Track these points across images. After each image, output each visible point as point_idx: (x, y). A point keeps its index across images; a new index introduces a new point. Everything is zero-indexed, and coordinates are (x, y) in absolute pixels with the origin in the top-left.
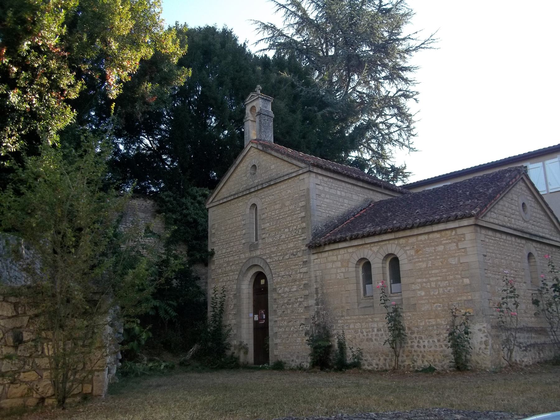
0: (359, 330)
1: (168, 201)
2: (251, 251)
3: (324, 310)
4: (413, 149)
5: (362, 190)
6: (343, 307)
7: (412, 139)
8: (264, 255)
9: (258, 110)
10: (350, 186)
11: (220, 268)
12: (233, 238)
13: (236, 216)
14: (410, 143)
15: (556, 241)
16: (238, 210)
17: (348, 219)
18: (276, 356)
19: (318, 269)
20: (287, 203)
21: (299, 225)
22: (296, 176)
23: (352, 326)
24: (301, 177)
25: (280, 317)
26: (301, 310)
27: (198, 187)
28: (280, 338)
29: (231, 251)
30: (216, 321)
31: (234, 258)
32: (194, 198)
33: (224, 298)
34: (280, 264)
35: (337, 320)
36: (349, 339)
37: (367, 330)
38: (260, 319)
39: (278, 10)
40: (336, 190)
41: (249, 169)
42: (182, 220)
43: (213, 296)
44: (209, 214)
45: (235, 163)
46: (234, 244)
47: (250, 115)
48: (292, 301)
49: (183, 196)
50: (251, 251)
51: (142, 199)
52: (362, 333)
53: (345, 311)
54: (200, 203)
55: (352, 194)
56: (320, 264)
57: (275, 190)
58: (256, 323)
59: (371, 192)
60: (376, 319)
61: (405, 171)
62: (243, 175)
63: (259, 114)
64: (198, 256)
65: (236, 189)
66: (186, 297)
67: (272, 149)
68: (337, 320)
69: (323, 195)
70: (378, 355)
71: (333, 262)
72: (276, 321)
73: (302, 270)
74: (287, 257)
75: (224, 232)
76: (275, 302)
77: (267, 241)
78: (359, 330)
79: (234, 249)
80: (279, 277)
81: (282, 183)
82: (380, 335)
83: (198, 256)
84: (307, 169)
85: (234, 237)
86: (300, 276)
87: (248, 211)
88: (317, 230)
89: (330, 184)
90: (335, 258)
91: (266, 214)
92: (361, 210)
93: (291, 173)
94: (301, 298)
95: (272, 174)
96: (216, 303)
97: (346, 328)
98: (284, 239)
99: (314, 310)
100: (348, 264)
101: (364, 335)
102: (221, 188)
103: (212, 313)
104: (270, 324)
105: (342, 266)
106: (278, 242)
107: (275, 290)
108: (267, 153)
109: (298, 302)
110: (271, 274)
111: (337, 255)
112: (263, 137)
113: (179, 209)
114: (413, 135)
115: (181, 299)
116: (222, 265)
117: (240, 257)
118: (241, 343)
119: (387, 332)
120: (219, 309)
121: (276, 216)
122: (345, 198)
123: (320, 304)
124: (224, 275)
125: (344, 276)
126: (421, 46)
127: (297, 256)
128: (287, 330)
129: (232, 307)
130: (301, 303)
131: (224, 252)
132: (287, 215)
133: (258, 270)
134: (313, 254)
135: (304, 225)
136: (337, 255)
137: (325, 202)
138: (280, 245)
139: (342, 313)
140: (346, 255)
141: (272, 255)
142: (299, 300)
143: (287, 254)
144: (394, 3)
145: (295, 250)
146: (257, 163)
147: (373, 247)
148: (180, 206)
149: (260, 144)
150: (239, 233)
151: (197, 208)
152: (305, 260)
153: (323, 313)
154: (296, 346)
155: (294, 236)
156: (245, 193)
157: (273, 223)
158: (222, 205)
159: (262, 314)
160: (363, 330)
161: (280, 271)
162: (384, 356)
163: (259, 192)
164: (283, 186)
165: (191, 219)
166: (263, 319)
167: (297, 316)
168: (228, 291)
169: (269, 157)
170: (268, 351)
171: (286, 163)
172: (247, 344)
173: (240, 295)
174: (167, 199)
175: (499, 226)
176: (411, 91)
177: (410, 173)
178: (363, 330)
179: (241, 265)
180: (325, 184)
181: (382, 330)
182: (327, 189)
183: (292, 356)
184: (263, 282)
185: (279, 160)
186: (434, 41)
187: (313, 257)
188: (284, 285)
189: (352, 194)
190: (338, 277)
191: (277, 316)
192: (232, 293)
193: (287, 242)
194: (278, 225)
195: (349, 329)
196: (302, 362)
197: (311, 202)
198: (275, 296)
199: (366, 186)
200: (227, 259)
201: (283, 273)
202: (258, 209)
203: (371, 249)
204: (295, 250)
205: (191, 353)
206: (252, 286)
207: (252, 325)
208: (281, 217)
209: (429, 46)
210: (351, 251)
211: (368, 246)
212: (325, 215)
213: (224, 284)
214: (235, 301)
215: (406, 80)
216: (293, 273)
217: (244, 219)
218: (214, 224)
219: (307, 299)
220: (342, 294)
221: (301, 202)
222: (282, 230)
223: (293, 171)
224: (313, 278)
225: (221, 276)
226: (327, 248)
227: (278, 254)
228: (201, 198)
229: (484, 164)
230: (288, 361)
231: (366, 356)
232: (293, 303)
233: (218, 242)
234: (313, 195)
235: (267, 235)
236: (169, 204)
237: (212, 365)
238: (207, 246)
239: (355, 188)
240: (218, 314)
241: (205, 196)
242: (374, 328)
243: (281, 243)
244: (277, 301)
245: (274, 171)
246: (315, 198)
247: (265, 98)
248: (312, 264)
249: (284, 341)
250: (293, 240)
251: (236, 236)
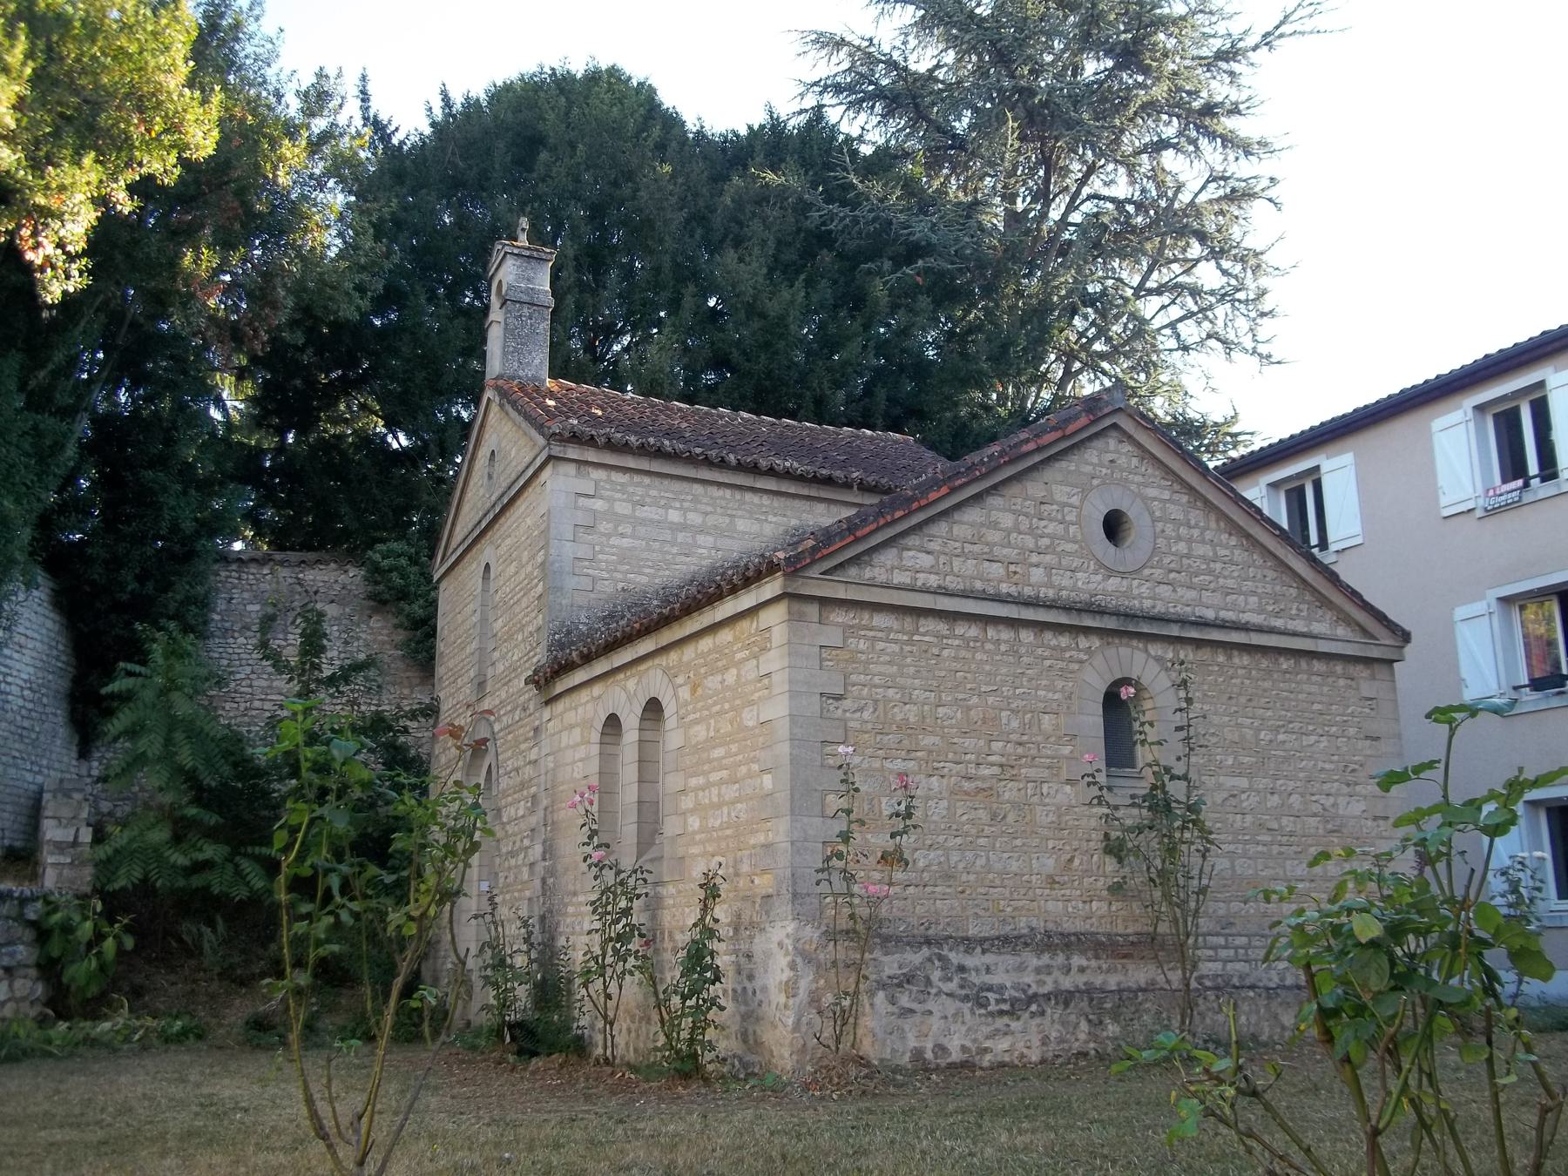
5: (778, 503)
7: (1266, 327)
15: (1295, 634)
51: (333, 565)
55: (730, 516)
57: (509, 523)
61: (1234, 430)
89: (640, 491)
122: (702, 530)
126: (1281, 30)
137: (613, 546)
175: (927, 596)
177: (1252, 434)
182: (623, 508)
189: (730, 516)
199: (792, 488)
209: (1308, 25)
212: (607, 588)
215: (1228, 140)
236: (394, 575)
239: (749, 496)
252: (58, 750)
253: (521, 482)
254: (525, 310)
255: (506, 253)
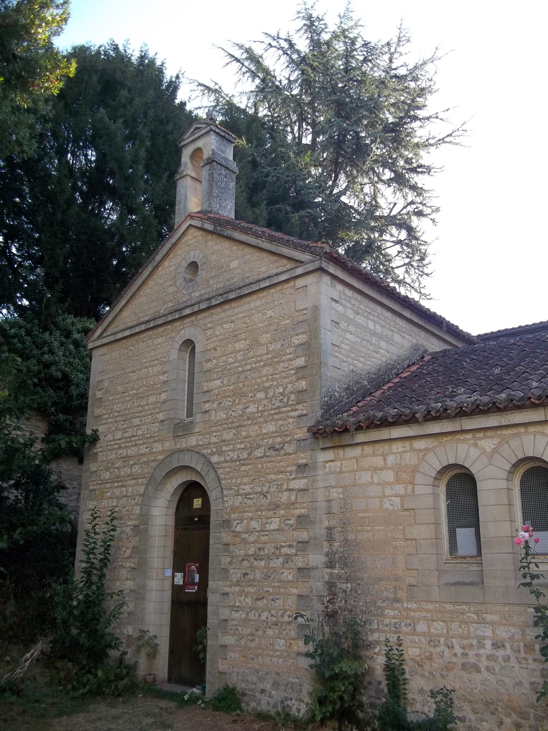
0: (442, 640)
1: (15, 336)
2: (176, 437)
3: (347, 580)
4: (425, 295)
5: (409, 327)
6: (397, 579)
7: (424, 281)
8: (206, 446)
9: (206, 154)
10: (389, 315)
11: (107, 469)
12: (140, 409)
13: (148, 364)
14: (421, 286)
16: (153, 353)
17: (389, 382)
18: (222, 673)
19: (334, 484)
20: (265, 338)
21: (290, 386)
22: (286, 281)
23: (421, 627)
24: (300, 282)
25: (236, 586)
26: (288, 575)
27: (75, 316)
28: (234, 634)
29: (133, 436)
30: (92, 584)
31: (138, 450)
32: (68, 334)
33: (112, 533)
34: (243, 468)
35: (383, 609)
36: (413, 660)
37: (465, 642)
38: (188, 582)
39: (227, 64)
40: (366, 317)
41: (182, 270)
42: (39, 373)
43: (89, 527)
44: (93, 364)
45: (154, 259)
46: (141, 421)
47: (190, 165)
48: (266, 551)
49: (45, 329)
50: (176, 437)
52: (451, 647)
53: (405, 589)
54: (77, 344)
55: (392, 331)
56: (341, 472)
57: (237, 311)
58: (176, 590)
59: (423, 334)
60: (489, 617)
62: (169, 283)
63: (210, 161)
64: (63, 443)
65: (151, 312)
66: (29, 528)
67: (235, 228)
68: (381, 607)
69: (343, 325)
70: (497, 710)
71: (376, 469)
72: (226, 594)
73: (292, 485)
74: (258, 453)
75: (122, 397)
76: (227, 550)
77: (213, 416)
78: (442, 640)
79: (140, 432)
80: (236, 495)
81: (254, 297)
82: (500, 659)
83: (63, 443)
84: (316, 265)
85: (142, 407)
86: (289, 498)
87: (174, 354)
88: (331, 398)
89: (357, 303)
90: (379, 461)
91: (214, 361)
92: (409, 366)
93: (277, 274)
94: (290, 546)
95: (233, 278)
96: (95, 543)
97: (404, 629)
98: (253, 413)
99: (323, 577)
100: (413, 477)
101: (455, 655)
102: (121, 310)
103: (84, 565)
104: (212, 598)
105: (398, 481)
106: (239, 421)
107: (227, 523)
108: (222, 236)
109: (281, 555)
110: (219, 488)
111: (384, 456)
112: (215, 207)
113: (35, 352)
114: (427, 275)
115: (18, 531)
116: (113, 464)
117: (152, 449)
118: (144, 632)
119: (522, 654)
120: (100, 557)
121: (237, 364)
123: (337, 565)
124: (116, 484)
125: (402, 504)
127: (283, 452)
128: (251, 616)
129: (128, 552)
130: (288, 558)
131: (117, 437)
132: (262, 364)
133: (194, 479)
134: (324, 449)
135: (303, 384)
136: (384, 456)
137: (347, 339)
138: (244, 426)
139: (395, 592)
140: (407, 456)
141: (224, 448)
142: (284, 550)
143: (258, 447)
144: (411, 67)
145: (279, 440)
146: (201, 257)
147: (480, 439)
148: (37, 347)
149: (209, 219)
150: (152, 399)
151: (70, 354)
152: (302, 461)
153: (344, 586)
154: (272, 656)
155: (279, 407)
156: (170, 318)
157: (229, 381)
158: (120, 343)
159: (193, 571)
160: (454, 641)
161: (240, 484)
162: (514, 716)
163: (200, 316)
164: (255, 302)
165: (59, 373)
166: (193, 584)
167: (279, 587)
168: (121, 519)
169: (226, 244)
170: (205, 658)
171: (265, 255)
172: (155, 636)
173: (146, 530)
174: (13, 331)
176: (428, 205)
178: (454, 641)
179: (154, 464)
180: (348, 301)
181: (507, 645)
182: (350, 314)
183: (261, 679)
184: (197, 503)
185: (248, 250)
186: (466, 133)
187: (322, 456)
188: (250, 515)
189: (392, 331)
190: (387, 505)
191: (228, 583)
192: (129, 523)
193: (259, 420)
194: (241, 385)
195: (414, 632)
196: (286, 698)
197: (322, 336)
198: (226, 537)
200: (124, 452)
201: (247, 489)
202: (197, 350)
203: (476, 445)
204: (279, 440)
205: (27, 664)
206: (173, 511)
207: (168, 595)
208: (249, 367)
209: (457, 140)
210: (423, 447)
211: (469, 436)
212: (346, 368)
213: (114, 504)
214: (135, 541)
216: (272, 489)
217: (164, 370)
218: (102, 381)
219: (304, 551)
220: (395, 548)
221: (297, 335)
222: (250, 395)
223: (280, 270)
224: (322, 505)
225: (109, 485)
226: (361, 437)
227: (238, 446)
228: (79, 335)
229: (527, 326)
230: (252, 690)
231: (461, 709)
232: (269, 557)
233: (107, 416)
234: (325, 321)
235: (215, 405)
237: (74, 689)
238: (84, 425)
240: (98, 567)
241: (86, 331)
242: (484, 638)
243: (245, 423)
244: (231, 548)
245: (236, 272)
246: (329, 327)
247: (223, 134)
248: (320, 472)
249: (242, 643)
250: (276, 417)
251: (147, 404)
252: (25, 521)
253: (255, 287)
254: (223, 171)
255: (211, 130)
